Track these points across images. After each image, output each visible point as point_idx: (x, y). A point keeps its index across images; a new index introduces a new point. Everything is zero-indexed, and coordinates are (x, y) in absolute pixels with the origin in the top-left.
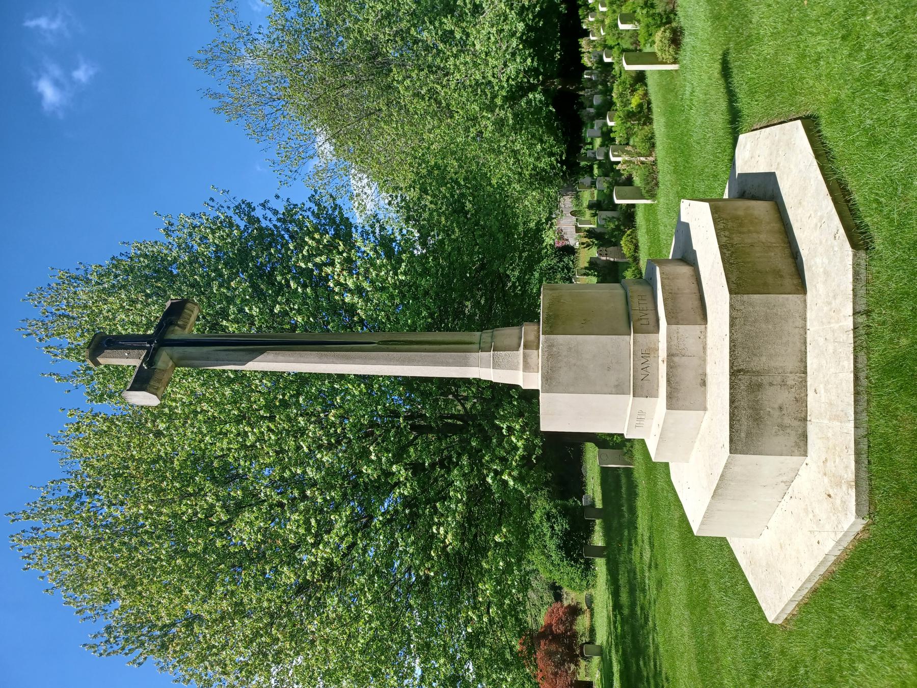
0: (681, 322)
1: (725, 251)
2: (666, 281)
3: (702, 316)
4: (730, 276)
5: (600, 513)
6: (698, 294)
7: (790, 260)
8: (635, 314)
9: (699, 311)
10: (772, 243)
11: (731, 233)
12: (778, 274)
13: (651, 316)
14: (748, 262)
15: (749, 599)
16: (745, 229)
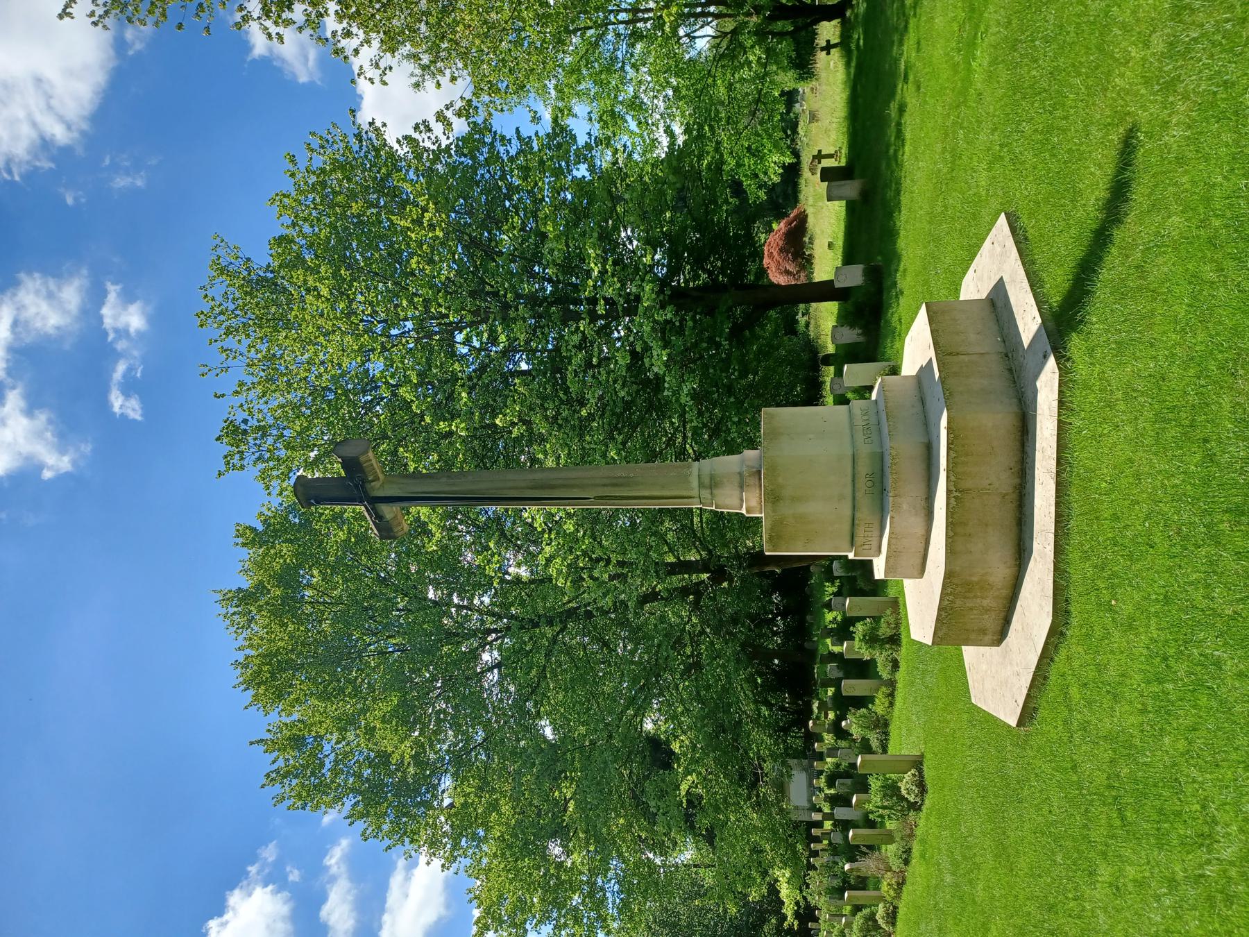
6: (922, 553)
13: (874, 543)
16: (971, 595)
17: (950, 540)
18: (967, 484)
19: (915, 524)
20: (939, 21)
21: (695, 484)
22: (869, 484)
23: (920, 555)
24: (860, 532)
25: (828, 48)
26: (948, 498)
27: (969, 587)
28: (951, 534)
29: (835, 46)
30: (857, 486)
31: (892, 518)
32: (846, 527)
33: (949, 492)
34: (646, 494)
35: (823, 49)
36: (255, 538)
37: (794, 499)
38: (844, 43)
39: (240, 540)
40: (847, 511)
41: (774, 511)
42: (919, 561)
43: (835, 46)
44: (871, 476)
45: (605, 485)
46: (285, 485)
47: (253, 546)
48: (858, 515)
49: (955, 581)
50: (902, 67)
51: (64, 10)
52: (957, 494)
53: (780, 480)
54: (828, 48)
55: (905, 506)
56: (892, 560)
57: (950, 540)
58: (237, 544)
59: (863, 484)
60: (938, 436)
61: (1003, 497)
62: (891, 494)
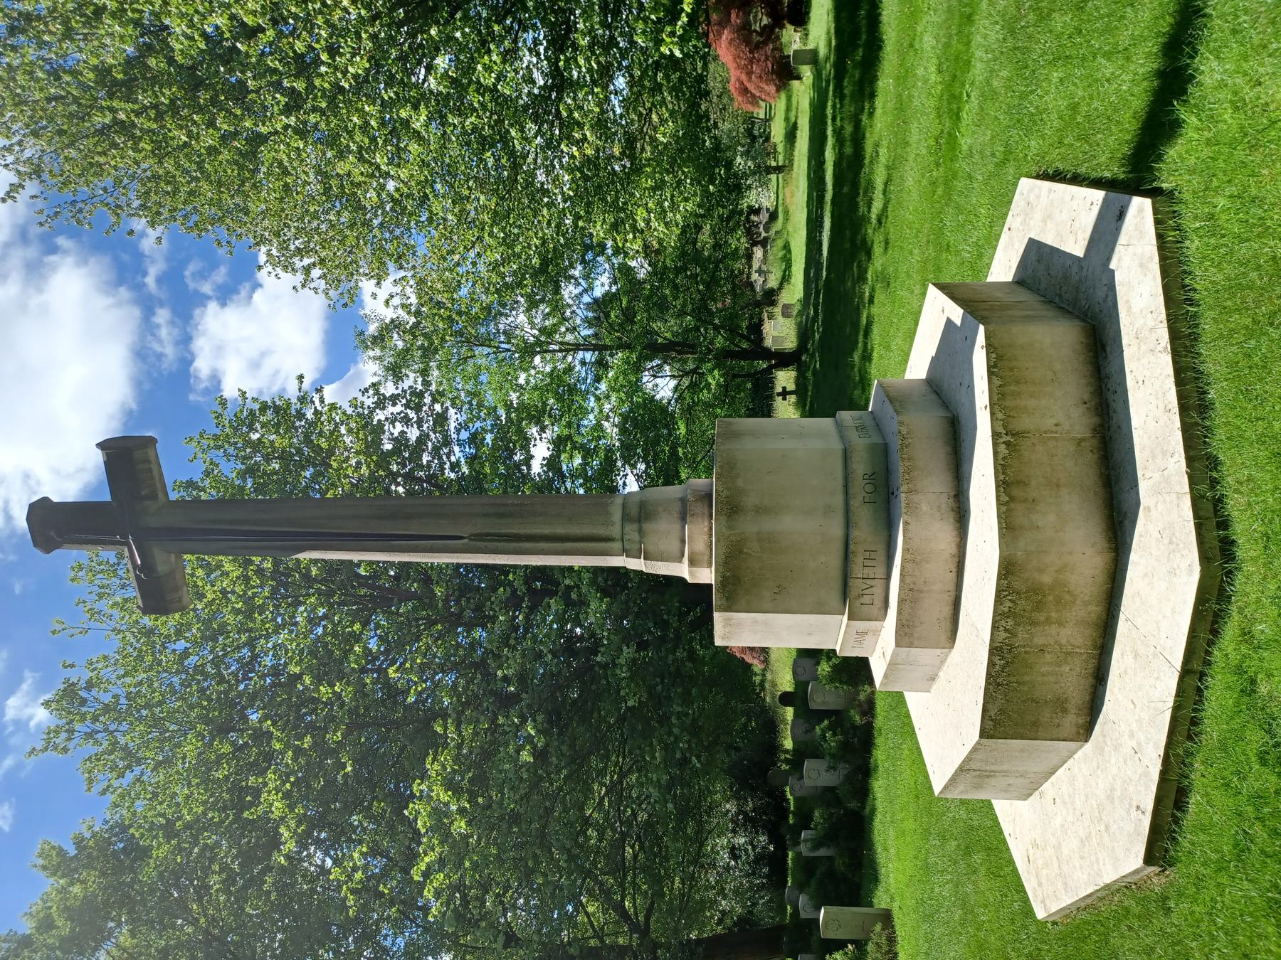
0: (916, 643)
1: (996, 659)
2: (909, 566)
3: (949, 634)
4: (990, 706)
5: (792, 812)
6: (953, 594)
7: (1091, 680)
8: (856, 585)
9: (947, 625)
10: (1073, 646)
11: (1017, 624)
12: (1060, 705)
13: (878, 591)
14: (1024, 683)
15: (930, 787)
16: (1041, 617)
17: (1004, 508)
18: (1023, 423)
19: (941, 535)
20: (910, 182)
21: (617, 515)
22: (869, 488)
23: (949, 598)
24: (858, 570)
25: (784, 394)
26: (995, 445)
27: (1037, 595)
28: (1005, 498)
29: (791, 393)
30: (851, 491)
31: (906, 523)
32: (835, 562)
33: (996, 435)
34: (546, 531)
35: (779, 394)
36: (61, 865)
37: (761, 511)
38: (800, 390)
39: (41, 862)
40: (837, 530)
41: (730, 528)
42: (947, 610)
43: (791, 393)
44: (871, 478)
45: (486, 515)
46: (115, 783)
47: (54, 874)
48: (855, 533)
49: (1017, 585)
50: (864, 320)
51: (8, 194)
52: (1009, 438)
53: (740, 483)
54: (784, 394)
55: (925, 507)
56: (906, 607)
57: (1004, 508)
58: (35, 866)
59: (860, 489)
60: (971, 387)
61: (1079, 444)
62: (902, 489)
